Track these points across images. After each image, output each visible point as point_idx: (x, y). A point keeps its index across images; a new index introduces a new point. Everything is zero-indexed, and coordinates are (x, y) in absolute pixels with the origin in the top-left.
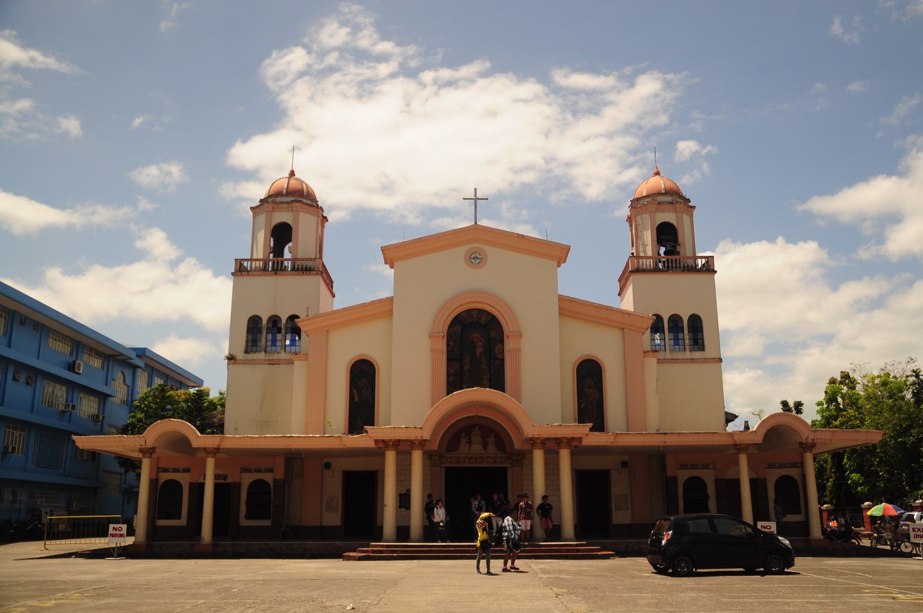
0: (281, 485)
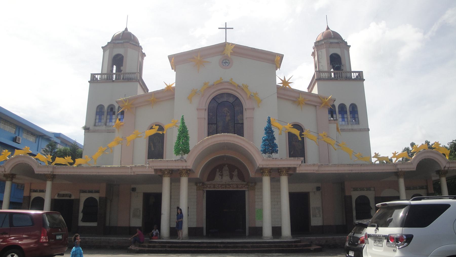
0: (104, 201)
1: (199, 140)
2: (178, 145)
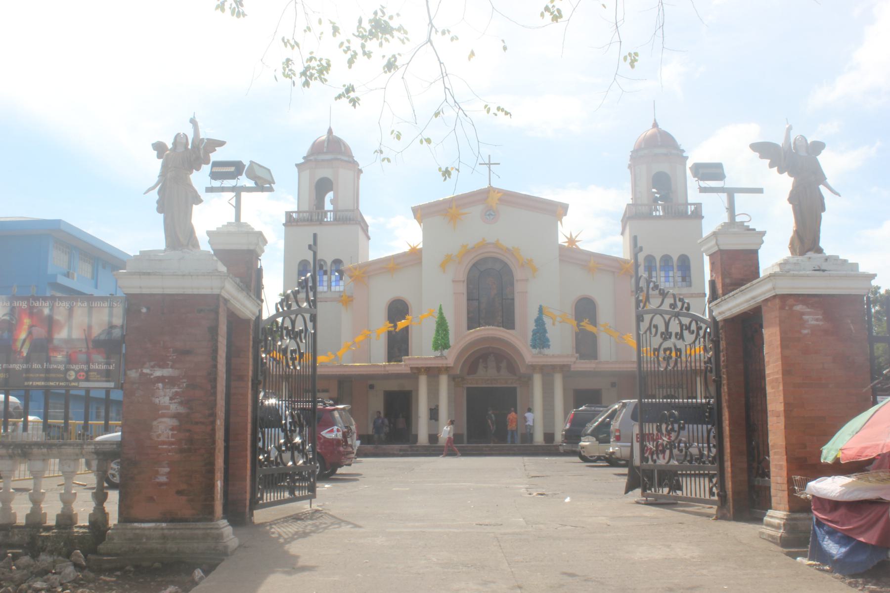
1: (461, 337)
2: (436, 340)
